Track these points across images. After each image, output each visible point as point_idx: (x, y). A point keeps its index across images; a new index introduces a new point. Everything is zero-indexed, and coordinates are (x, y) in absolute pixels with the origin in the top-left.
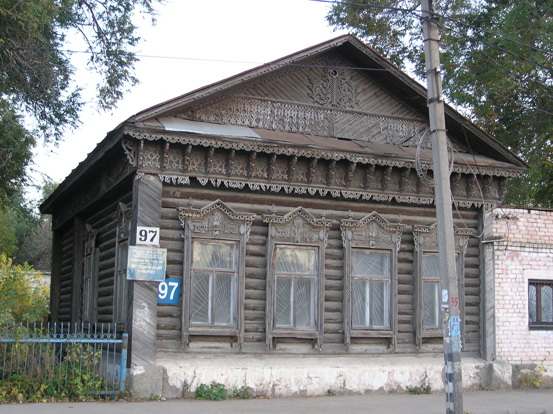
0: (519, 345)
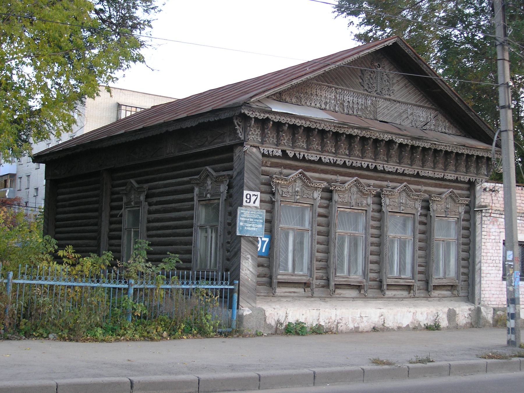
0: (496, 292)
